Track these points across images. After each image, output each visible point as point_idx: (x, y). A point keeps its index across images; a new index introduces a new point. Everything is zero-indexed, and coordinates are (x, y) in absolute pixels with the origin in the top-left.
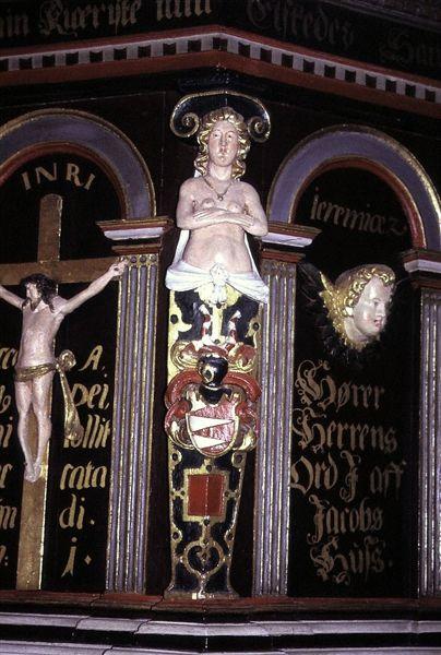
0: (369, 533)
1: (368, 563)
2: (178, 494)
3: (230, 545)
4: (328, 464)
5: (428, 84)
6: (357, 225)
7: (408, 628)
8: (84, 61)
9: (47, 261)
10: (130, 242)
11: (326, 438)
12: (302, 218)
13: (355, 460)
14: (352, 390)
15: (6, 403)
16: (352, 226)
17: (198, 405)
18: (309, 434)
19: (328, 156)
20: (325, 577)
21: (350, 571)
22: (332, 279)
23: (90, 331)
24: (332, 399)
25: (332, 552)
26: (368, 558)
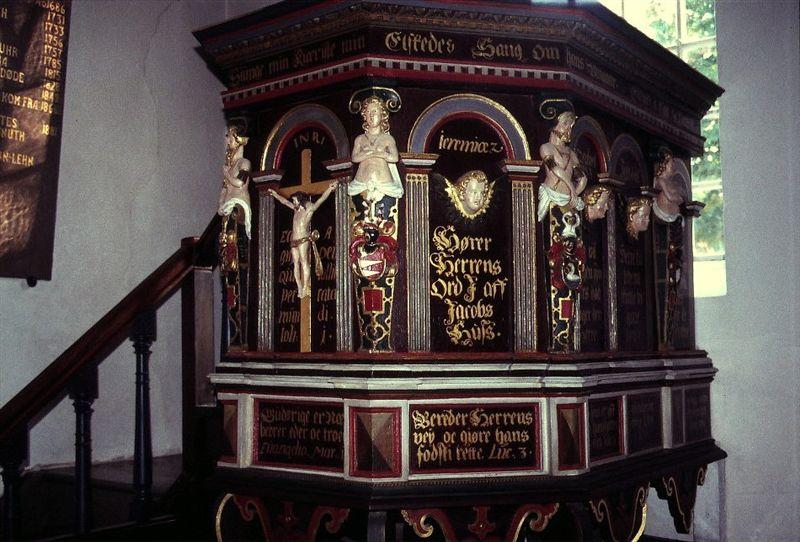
0: (484, 318)
3: (389, 325)
4: (456, 282)
6: (469, 149)
7: (516, 367)
8: (320, 76)
9: (306, 185)
10: (339, 171)
11: (454, 268)
13: (474, 279)
14: (470, 242)
17: (364, 254)
18: (443, 266)
19: (447, 113)
20: (456, 342)
21: (472, 339)
22: (454, 182)
23: (324, 220)
24: (457, 247)
25: (460, 329)
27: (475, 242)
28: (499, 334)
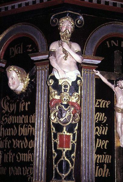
2: (74, 142)
5: (5, 5)
12: (97, 54)
15: (105, 119)
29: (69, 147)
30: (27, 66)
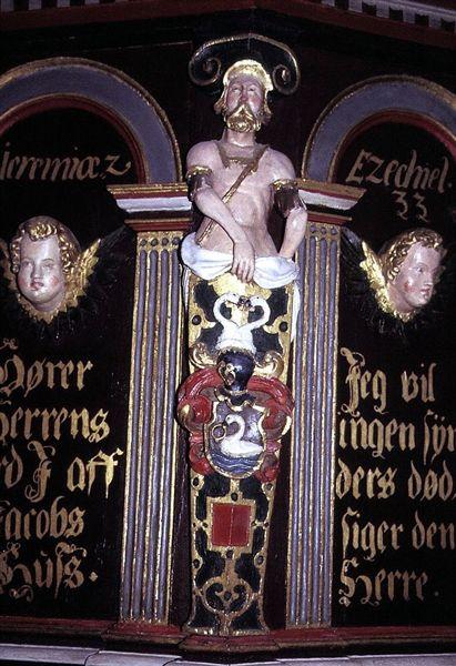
0: (63, 538)
1: (59, 577)
13: (48, 452)
14: (46, 370)
16: (53, 178)
22: (378, 249)
24: (19, 382)
26: (59, 571)
27: (58, 372)
28: (94, 576)
29: (219, 508)
30: (89, 217)
